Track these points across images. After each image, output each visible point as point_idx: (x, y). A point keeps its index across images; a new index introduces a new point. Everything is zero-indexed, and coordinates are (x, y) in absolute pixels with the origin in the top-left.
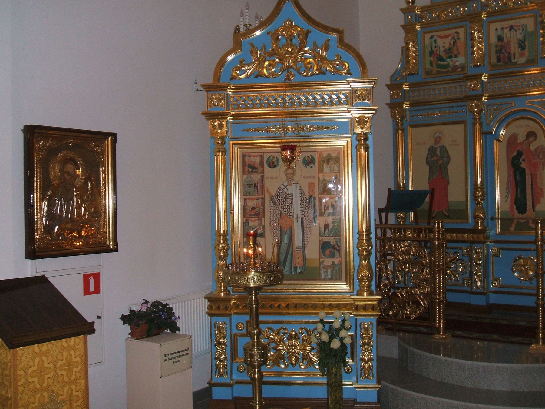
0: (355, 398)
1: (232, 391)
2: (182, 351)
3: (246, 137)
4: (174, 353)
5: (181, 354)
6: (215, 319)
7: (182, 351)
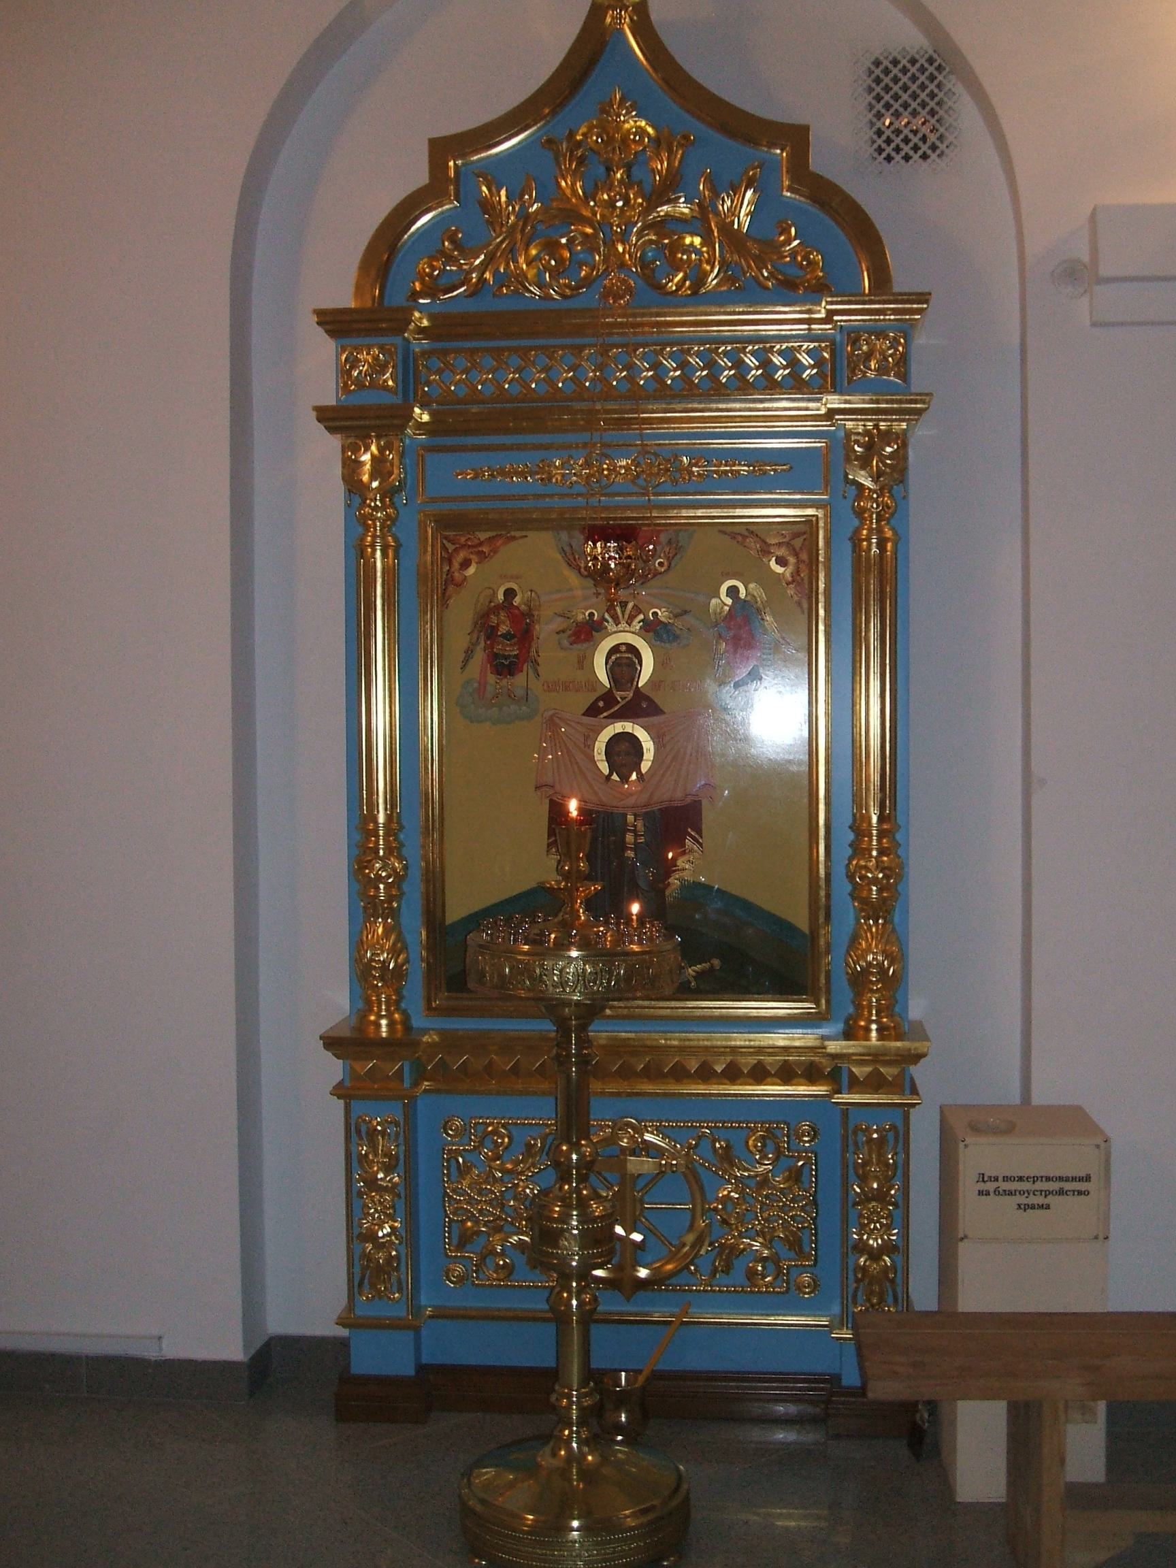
0: (837, 1371)
1: (418, 1350)
2: (1061, 1179)
3: (1034, 549)
4: (1021, 1179)
5: (1054, 1186)
6: (358, 1107)
7: (1061, 1179)
